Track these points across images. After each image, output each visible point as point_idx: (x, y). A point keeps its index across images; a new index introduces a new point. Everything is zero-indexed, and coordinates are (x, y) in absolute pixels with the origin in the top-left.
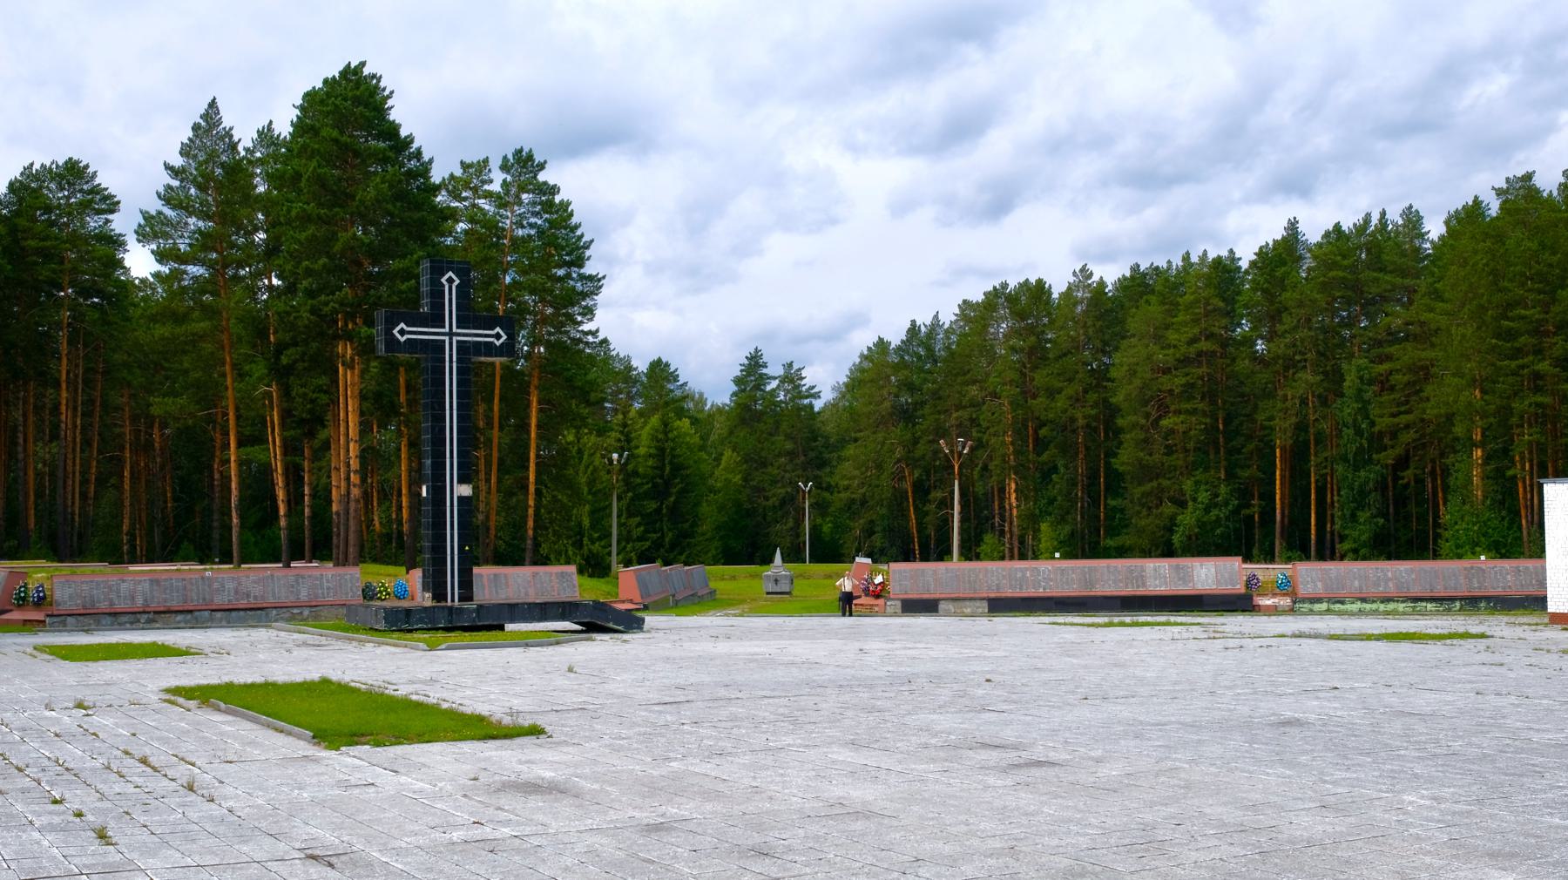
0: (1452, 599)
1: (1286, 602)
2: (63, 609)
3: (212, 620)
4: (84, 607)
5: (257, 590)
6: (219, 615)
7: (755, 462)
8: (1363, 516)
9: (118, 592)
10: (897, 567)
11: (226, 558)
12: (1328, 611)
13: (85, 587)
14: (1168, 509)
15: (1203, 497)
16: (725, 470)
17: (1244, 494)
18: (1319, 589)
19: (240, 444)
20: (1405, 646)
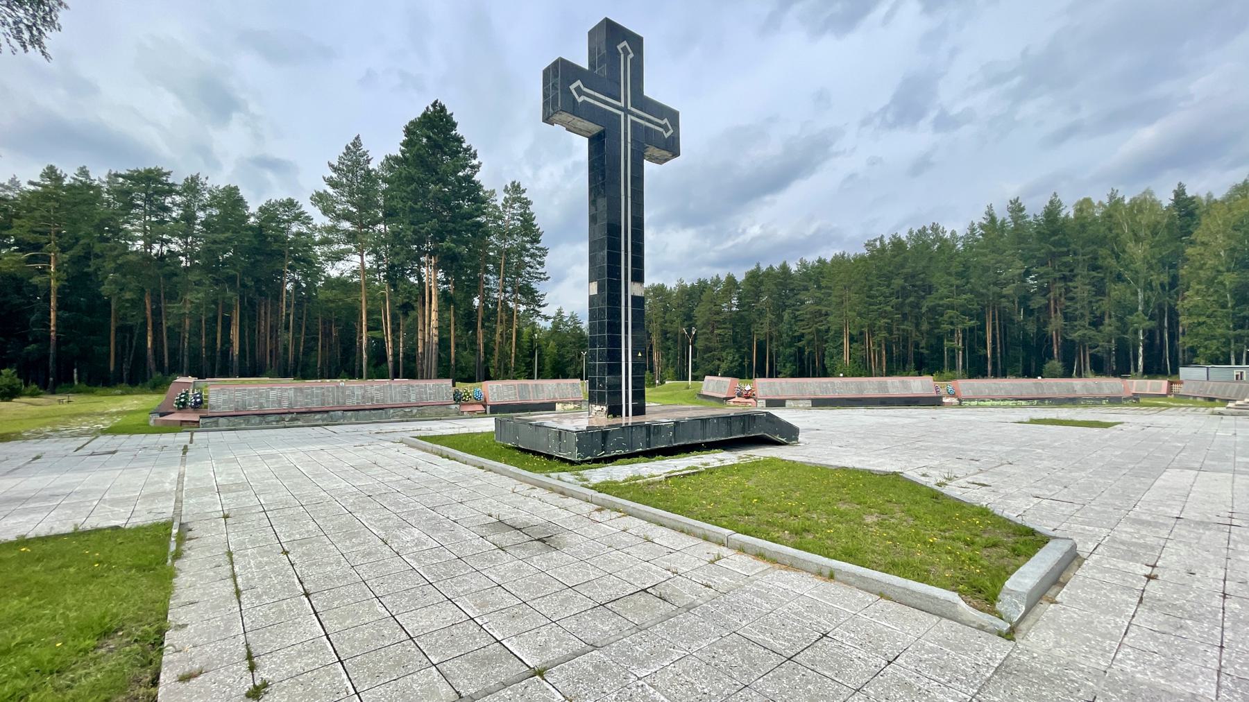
0: (1101, 399)
1: (955, 401)
2: (216, 412)
3: (344, 417)
4: (236, 410)
5: (379, 396)
6: (349, 414)
7: (561, 346)
8: (788, 365)
9: (268, 396)
10: (759, 381)
11: (361, 377)
12: (978, 406)
13: (237, 394)
14: (717, 362)
15: (730, 358)
16: (551, 348)
17: (742, 358)
18: (970, 394)
19: (368, 330)
20: (1096, 430)
